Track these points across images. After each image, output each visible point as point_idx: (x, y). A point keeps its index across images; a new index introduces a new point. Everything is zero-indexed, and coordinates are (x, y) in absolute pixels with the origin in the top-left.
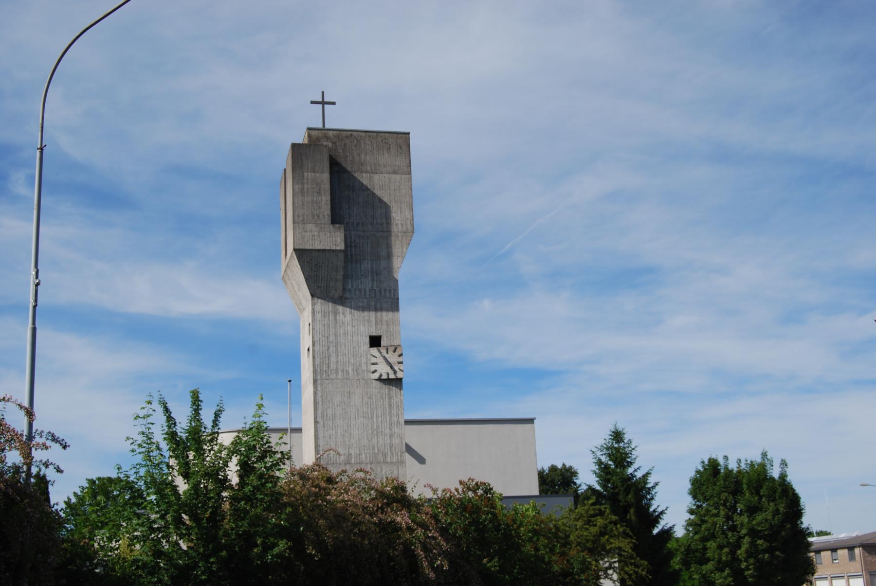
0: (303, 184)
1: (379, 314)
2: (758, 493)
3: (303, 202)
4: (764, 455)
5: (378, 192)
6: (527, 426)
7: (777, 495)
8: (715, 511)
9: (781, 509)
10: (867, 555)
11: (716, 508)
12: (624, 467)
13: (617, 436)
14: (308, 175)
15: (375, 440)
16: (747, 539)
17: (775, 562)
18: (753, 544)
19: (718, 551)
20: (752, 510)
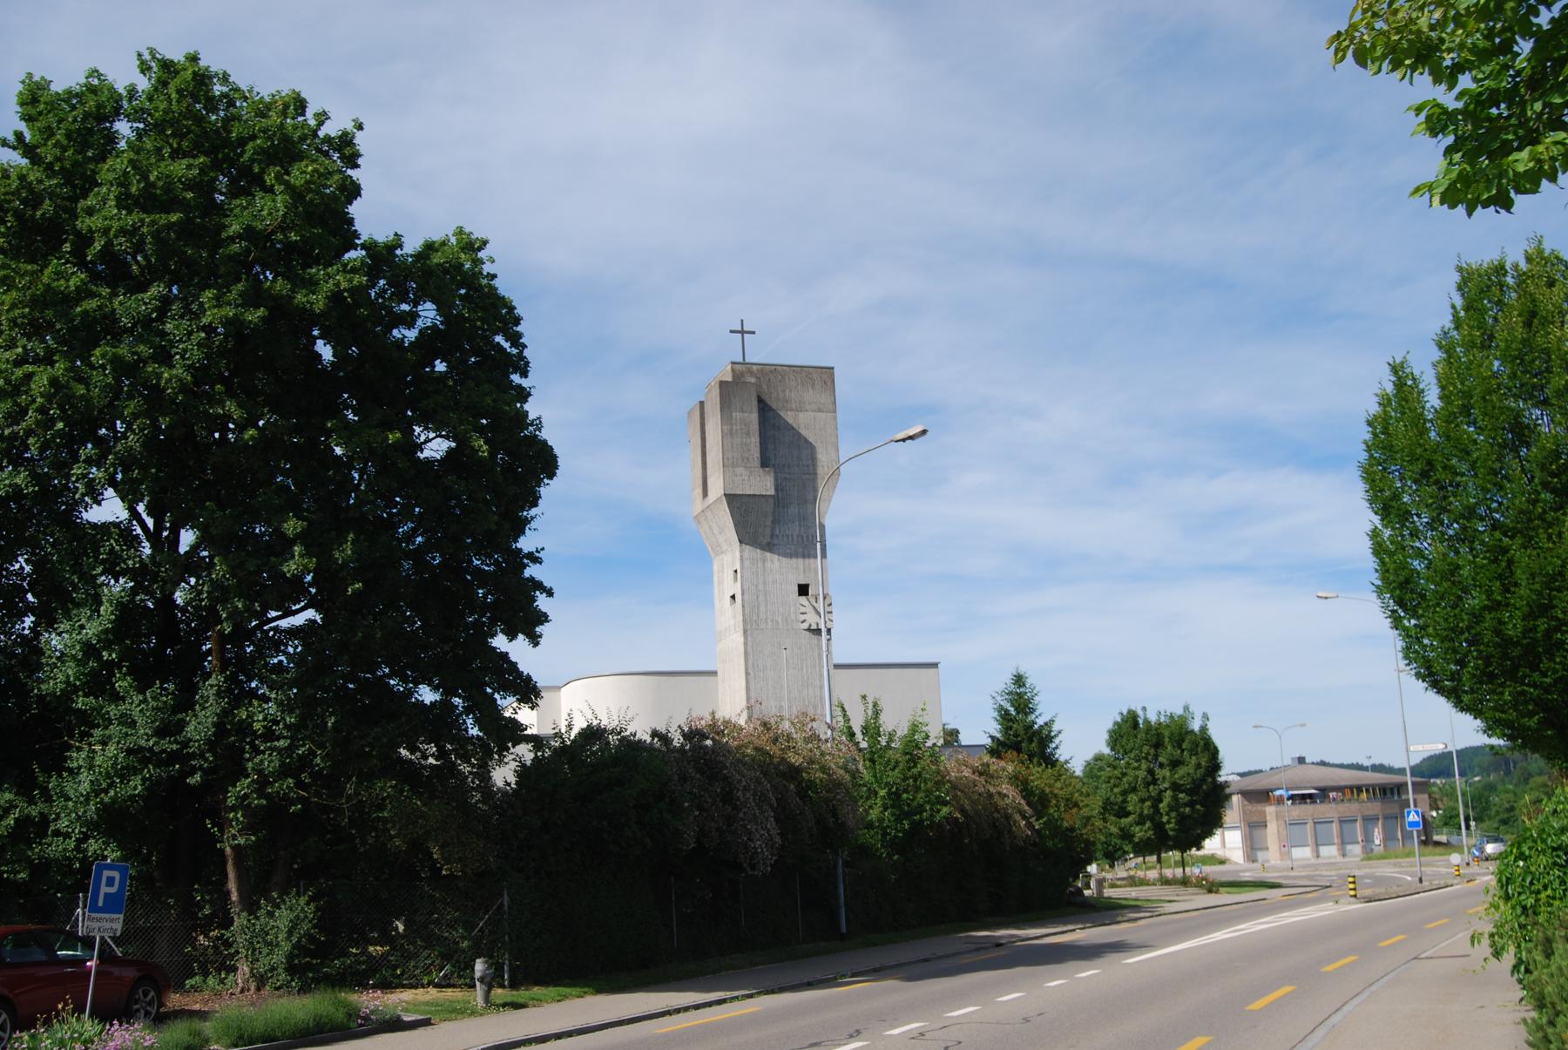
0: (731, 425)
1: (807, 560)
2: (1180, 746)
3: (732, 444)
4: (1186, 708)
5: (803, 432)
6: (931, 671)
7: (1199, 749)
8: (1136, 764)
9: (1203, 763)
10: (1246, 803)
11: (1136, 762)
12: (1026, 714)
13: (1019, 680)
14: (737, 415)
15: (805, 692)
16: (1169, 793)
17: (1195, 815)
18: (1175, 798)
19: (1140, 804)
20: (1175, 764)
